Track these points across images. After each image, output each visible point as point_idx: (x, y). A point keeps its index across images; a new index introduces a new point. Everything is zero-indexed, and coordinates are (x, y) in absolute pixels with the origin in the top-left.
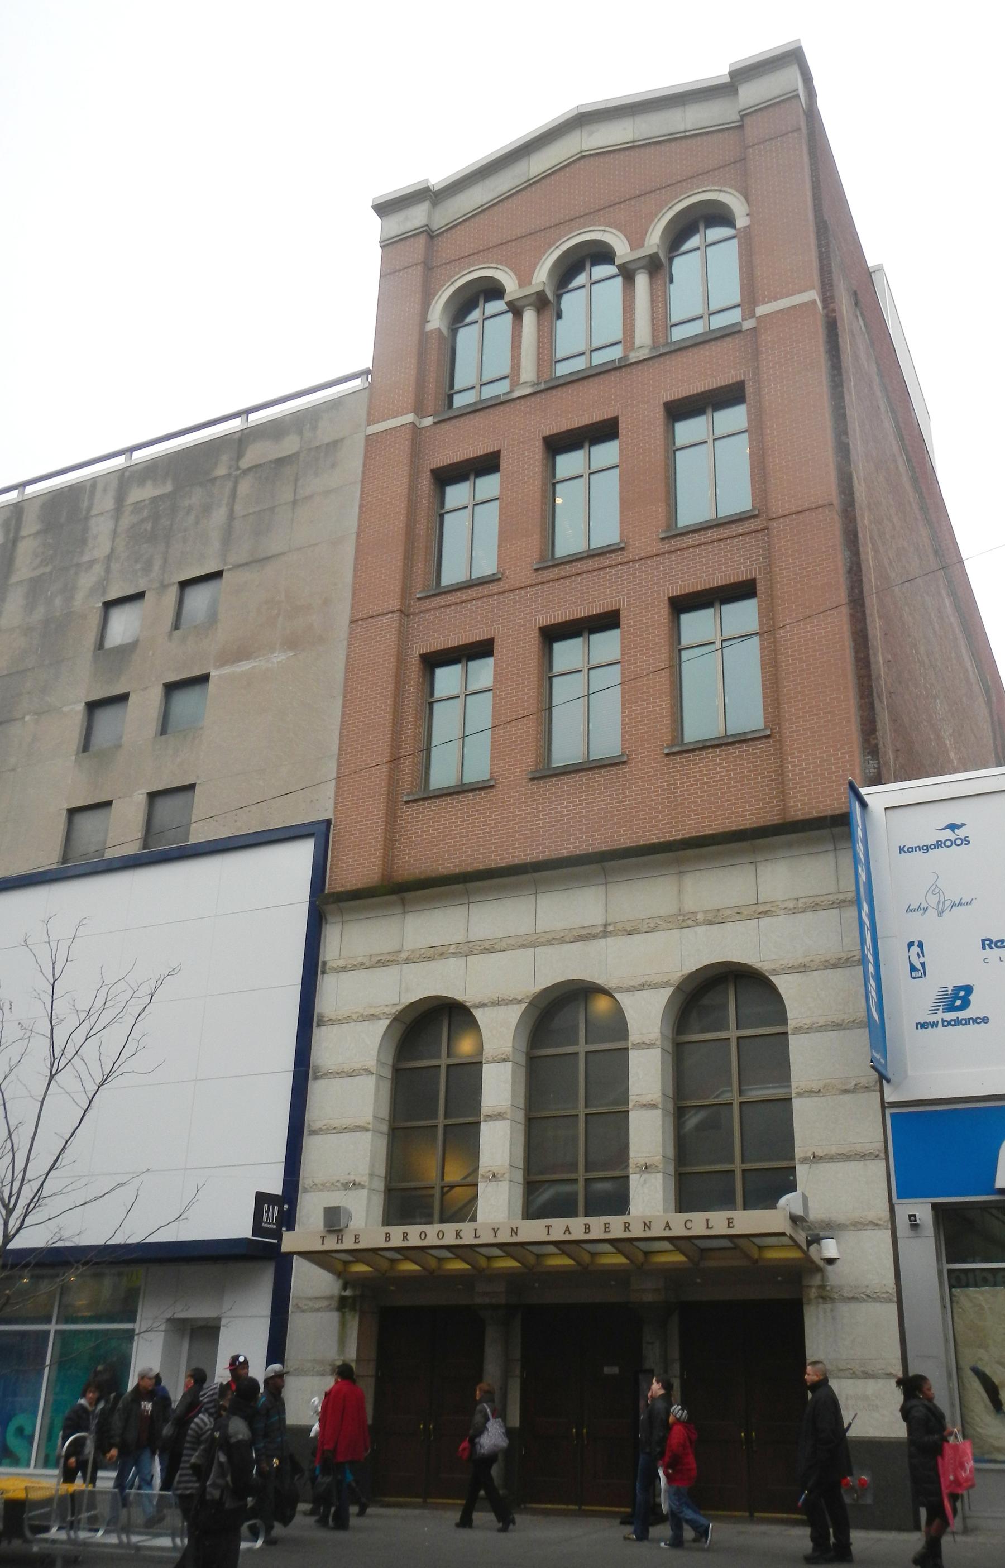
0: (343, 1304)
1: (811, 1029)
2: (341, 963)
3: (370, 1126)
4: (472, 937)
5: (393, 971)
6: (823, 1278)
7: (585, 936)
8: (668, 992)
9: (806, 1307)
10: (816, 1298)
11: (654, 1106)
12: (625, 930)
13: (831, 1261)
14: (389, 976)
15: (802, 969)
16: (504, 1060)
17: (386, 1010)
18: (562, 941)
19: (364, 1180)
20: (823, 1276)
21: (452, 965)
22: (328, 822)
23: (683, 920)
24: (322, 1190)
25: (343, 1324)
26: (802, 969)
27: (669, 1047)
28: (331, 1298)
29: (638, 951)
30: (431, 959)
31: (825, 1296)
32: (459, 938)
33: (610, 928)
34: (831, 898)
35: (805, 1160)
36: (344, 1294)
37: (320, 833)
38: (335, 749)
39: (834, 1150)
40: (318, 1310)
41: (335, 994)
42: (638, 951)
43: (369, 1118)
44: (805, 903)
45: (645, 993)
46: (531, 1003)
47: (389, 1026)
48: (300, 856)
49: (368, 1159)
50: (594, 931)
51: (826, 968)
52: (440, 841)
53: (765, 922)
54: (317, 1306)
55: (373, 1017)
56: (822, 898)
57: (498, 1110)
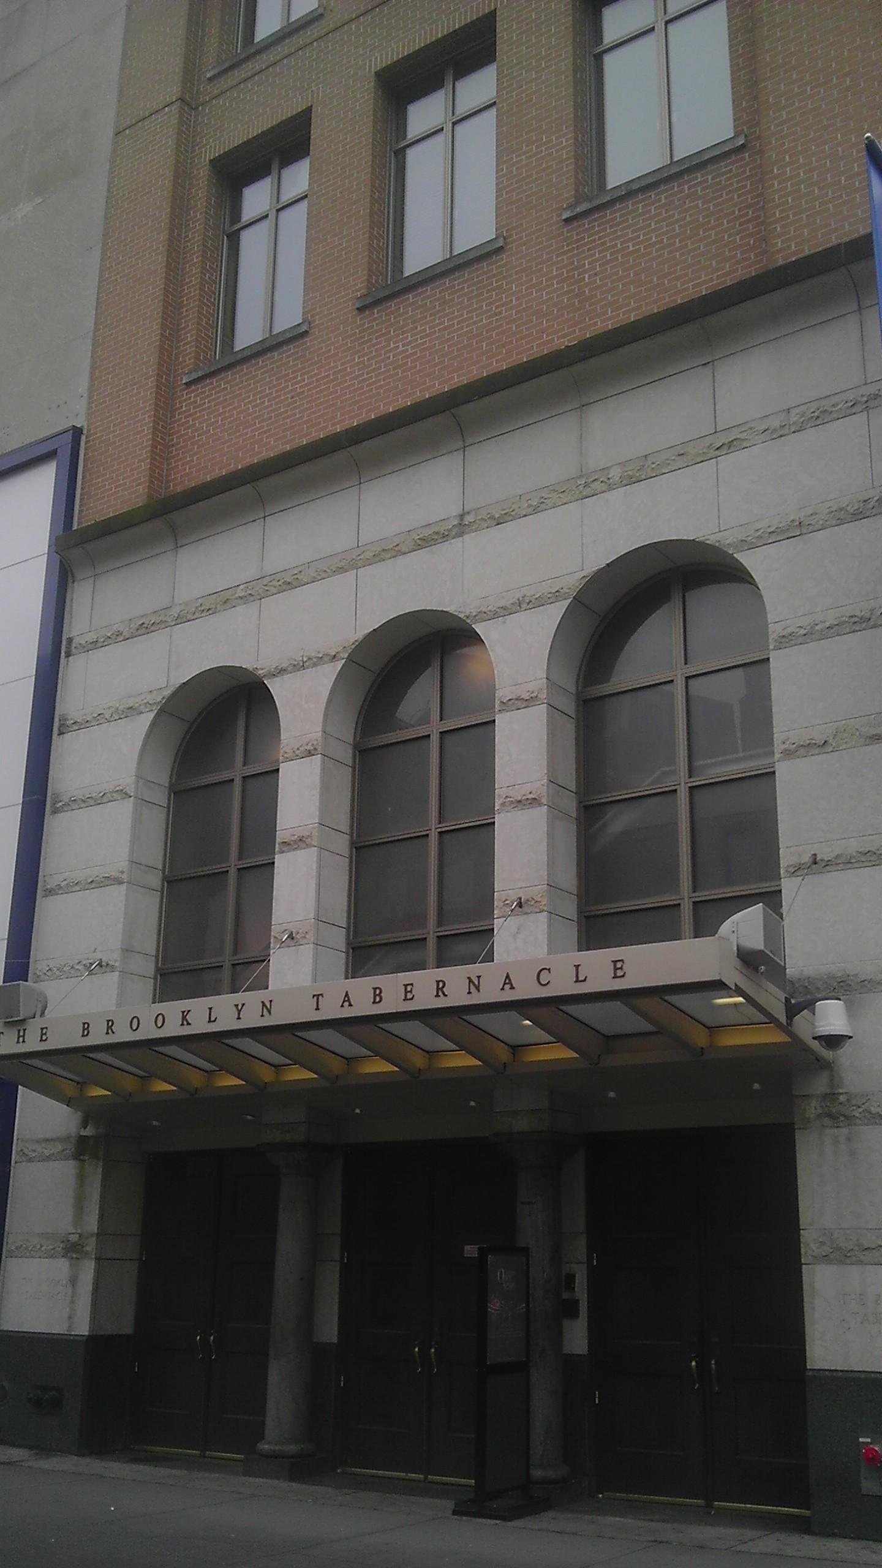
0: (82, 1148)
1: (811, 635)
2: (91, 637)
3: (125, 876)
4: (269, 569)
5: (159, 638)
6: (834, 1080)
7: (429, 540)
8: (559, 609)
9: (799, 1136)
10: (819, 1116)
11: (534, 802)
12: (492, 518)
13: (833, 1041)
14: (154, 645)
15: (795, 530)
16: (310, 754)
17: (150, 698)
18: (397, 552)
19: (114, 957)
20: (832, 1078)
21: (242, 617)
22: (77, 432)
23: (586, 485)
24: (59, 978)
25: (81, 1178)
26: (795, 530)
27: (569, 705)
28: (67, 1139)
29: (505, 548)
30: (210, 611)
31: (838, 1112)
32: (251, 573)
33: (469, 519)
34: (850, 395)
35: (797, 870)
36: (84, 1133)
37: (67, 452)
38: (91, 324)
39: (853, 846)
40: (48, 1158)
41: (85, 685)
42: (505, 548)
43: (124, 864)
44: (803, 415)
45: (521, 617)
46: (350, 659)
47: (154, 724)
48: (39, 488)
49: (121, 926)
50: (442, 528)
51: (841, 522)
52: (234, 428)
53: (726, 462)
54: (47, 1153)
55: (131, 711)
56: (835, 399)
57: (300, 832)
